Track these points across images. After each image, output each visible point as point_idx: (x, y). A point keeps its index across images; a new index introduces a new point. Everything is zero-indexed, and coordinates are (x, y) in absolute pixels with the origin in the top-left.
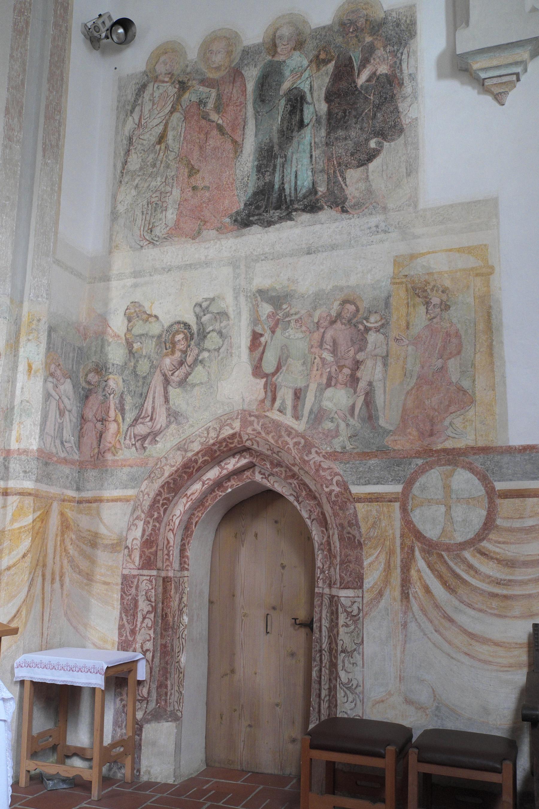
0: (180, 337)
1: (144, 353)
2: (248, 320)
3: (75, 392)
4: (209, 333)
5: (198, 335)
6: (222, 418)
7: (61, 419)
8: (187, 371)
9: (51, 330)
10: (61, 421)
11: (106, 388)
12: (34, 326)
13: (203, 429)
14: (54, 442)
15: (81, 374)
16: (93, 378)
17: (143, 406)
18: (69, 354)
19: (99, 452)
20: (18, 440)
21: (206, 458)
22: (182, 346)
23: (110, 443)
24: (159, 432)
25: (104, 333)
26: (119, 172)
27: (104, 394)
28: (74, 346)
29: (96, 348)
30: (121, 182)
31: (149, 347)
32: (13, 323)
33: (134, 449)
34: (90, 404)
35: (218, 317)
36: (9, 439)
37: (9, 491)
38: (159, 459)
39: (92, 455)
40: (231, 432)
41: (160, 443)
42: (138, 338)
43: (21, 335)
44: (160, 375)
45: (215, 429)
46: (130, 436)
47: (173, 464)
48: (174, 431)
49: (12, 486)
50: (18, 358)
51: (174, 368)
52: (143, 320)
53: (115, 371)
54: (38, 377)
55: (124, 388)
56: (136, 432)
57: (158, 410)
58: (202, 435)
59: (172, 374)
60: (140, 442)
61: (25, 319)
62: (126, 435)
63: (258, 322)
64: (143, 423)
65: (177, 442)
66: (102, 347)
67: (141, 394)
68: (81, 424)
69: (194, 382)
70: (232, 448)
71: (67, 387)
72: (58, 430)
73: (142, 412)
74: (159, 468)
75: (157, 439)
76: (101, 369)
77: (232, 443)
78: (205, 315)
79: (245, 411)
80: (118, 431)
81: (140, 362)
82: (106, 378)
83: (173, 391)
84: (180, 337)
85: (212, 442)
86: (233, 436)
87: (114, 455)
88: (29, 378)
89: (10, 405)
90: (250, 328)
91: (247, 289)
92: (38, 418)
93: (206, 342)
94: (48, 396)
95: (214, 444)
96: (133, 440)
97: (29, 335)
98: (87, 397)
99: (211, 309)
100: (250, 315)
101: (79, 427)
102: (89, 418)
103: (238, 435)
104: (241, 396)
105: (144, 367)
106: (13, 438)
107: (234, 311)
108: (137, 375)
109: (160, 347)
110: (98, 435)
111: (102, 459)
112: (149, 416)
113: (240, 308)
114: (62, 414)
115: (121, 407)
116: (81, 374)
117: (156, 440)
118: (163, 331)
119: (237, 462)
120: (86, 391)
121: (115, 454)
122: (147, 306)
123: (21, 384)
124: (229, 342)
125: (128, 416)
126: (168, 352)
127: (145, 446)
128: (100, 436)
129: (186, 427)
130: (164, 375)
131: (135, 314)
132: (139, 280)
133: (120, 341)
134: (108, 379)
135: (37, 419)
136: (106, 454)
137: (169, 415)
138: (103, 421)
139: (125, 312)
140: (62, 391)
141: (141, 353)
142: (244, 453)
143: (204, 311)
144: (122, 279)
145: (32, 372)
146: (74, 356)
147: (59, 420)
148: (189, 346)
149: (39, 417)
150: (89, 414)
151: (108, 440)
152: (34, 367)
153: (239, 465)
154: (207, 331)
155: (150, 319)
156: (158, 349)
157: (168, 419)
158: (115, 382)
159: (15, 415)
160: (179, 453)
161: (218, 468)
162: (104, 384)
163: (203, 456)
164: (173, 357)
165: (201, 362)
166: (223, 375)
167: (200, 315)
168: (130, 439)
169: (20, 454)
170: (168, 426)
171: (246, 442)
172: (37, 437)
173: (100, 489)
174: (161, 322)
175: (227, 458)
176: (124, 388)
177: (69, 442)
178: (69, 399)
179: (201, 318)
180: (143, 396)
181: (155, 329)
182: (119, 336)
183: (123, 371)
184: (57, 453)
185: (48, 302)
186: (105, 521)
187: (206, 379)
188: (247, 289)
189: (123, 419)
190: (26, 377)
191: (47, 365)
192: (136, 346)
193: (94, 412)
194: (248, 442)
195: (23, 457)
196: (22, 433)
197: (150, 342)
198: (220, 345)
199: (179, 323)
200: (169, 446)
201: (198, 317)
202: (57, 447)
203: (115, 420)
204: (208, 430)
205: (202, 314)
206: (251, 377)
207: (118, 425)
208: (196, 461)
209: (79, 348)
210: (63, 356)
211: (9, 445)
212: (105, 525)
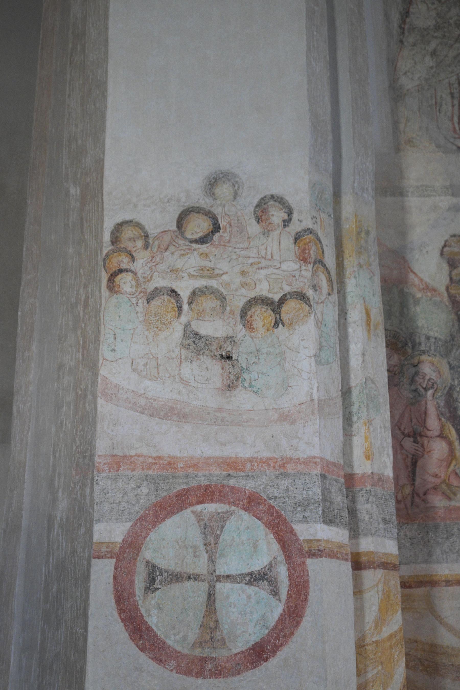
11: (417, 379)
19: (414, 493)
23: (436, 476)
26: (396, 25)
27: (413, 387)
30: (401, 41)
37: (364, 559)
39: (400, 498)
49: (371, 548)
53: (433, 348)
55: (453, 379)
82: (415, 361)
87: (450, 499)
115: (450, 412)
121: (452, 496)
134: (419, 363)
144: (429, 196)
162: (413, 370)
173: (426, 562)
182: (434, 290)
186: (451, 621)
203: (442, 436)
212: (450, 629)
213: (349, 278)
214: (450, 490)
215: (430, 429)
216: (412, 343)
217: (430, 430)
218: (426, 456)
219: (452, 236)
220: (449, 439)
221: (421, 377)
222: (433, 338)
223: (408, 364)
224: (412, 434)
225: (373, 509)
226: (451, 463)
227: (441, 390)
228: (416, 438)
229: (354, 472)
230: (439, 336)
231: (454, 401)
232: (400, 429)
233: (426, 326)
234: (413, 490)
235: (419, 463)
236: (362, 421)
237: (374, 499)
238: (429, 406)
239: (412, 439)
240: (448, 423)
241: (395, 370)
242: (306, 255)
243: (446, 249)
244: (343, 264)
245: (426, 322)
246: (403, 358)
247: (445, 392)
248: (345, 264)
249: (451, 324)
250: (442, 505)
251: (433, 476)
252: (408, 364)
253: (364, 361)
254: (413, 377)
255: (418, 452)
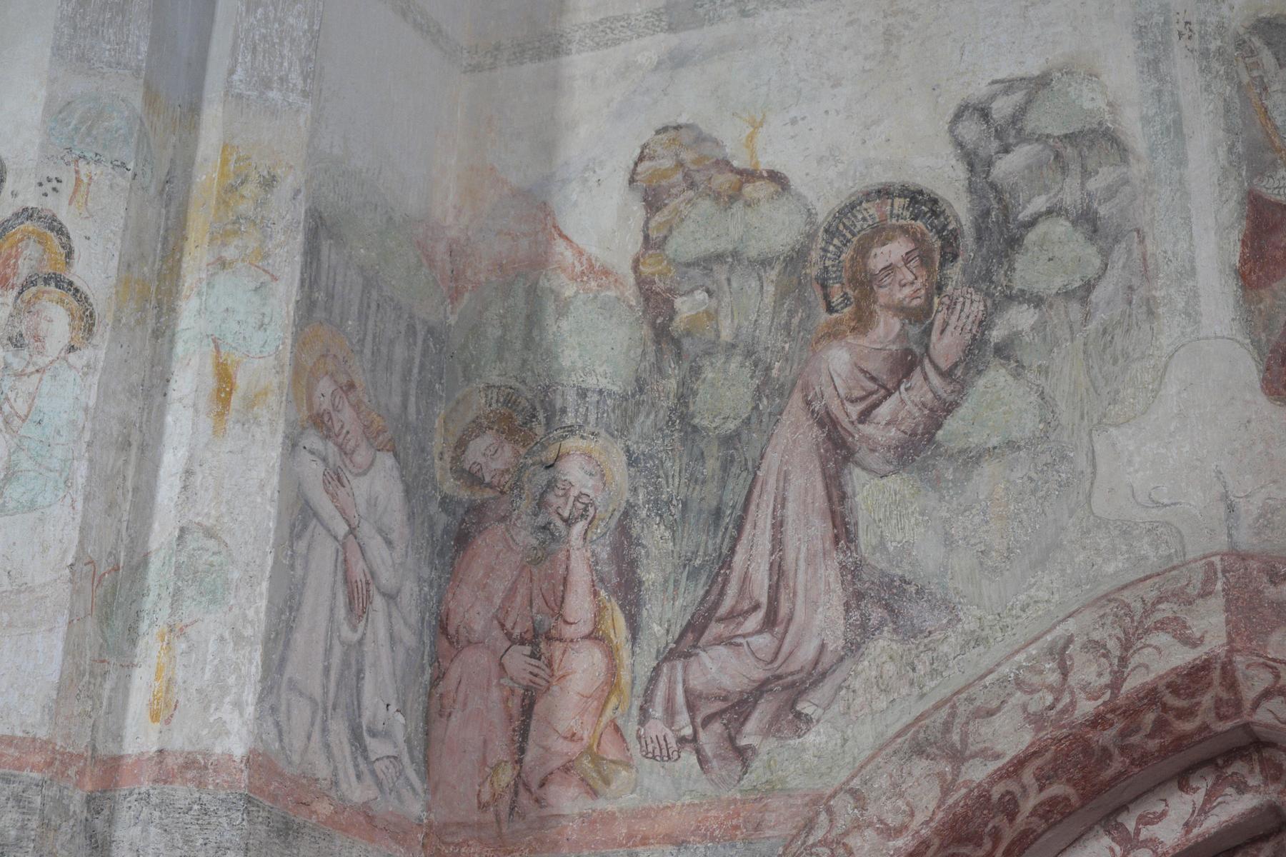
0: (894, 251)
1: (726, 335)
2: (1222, 152)
3: (411, 516)
4: (1032, 223)
5: (979, 239)
6: (1127, 596)
7: (354, 629)
8: (936, 396)
9: (320, 230)
10: (356, 637)
11: (551, 498)
12: (245, 207)
13: (1033, 650)
14: (325, 730)
15: (437, 443)
16: (491, 455)
17: (725, 562)
18: (392, 342)
19: (520, 783)
20: (163, 711)
21: (1057, 789)
22: (907, 291)
23: (572, 737)
24: (816, 675)
25: (539, 262)
27: (541, 520)
28: (411, 317)
29: (505, 327)
31: (749, 307)
32: (152, 191)
33: (689, 758)
34: (477, 571)
35: (1069, 152)
36: (118, 708)
38: (820, 803)
39: (486, 797)
40: (1182, 657)
41: (821, 727)
42: (695, 272)
43: (190, 246)
44: (806, 422)
45: (1096, 647)
46: (670, 700)
47: (892, 820)
48: (890, 668)
50: (172, 342)
51: (871, 386)
52: (717, 197)
53: (592, 418)
54: (259, 424)
55: (635, 490)
56: (697, 683)
57: (800, 578)
58: (1036, 680)
59: (865, 416)
60: (717, 727)
61: (207, 175)
62: (648, 696)
63: (1269, 156)
64: (729, 642)
65: (907, 719)
66: (533, 320)
67: (718, 514)
68: (435, 659)
69: (974, 440)
70: (1184, 736)
71: (379, 485)
72: (342, 675)
73: (722, 593)
74: (824, 842)
75: (805, 707)
76: (527, 417)
77: (1183, 714)
78: (1006, 150)
79: (1243, 557)
80: (612, 682)
81: (709, 374)
82: (550, 455)
83: (869, 492)
84: (894, 251)
85: (1087, 707)
86: (1196, 675)
87: (594, 793)
88: (219, 430)
89: (131, 551)
90: (1232, 184)
91: (1203, 23)
92: (256, 608)
93: (1020, 262)
94: (299, 517)
95: (1097, 721)
96: (683, 718)
97: (224, 244)
98: (463, 539)
99: (1033, 122)
100: (1228, 130)
101: (428, 671)
102: (470, 630)
103: (1216, 675)
104: (1218, 488)
105: (725, 394)
106: (138, 703)
107: (1146, 120)
108: (695, 429)
109: (802, 301)
110: (515, 704)
111: (533, 815)
112: (756, 607)
113: (1176, 106)
114: (357, 604)
115: (620, 574)
116: (437, 443)
117: (798, 715)
118: (811, 236)
119: (1204, 811)
120: (461, 511)
121: (599, 785)
122: (732, 140)
123: (183, 452)
124: (1136, 254)
125: (657, 610)
126: (838, 322)
127: (742, 742)
128: (527, 708)
129: (945, 648)
130: (827, 422)
131: (679, 176)
132: (691, 38)
133: (612, 293)
134: (558, 458)
135: (251, 614)
136: (552, 789)
137: (860, 596)
138: (539, 639)
139: (634, 172)
140: (361, 501)
141: (712, 336)
142: (1238, 767)
143: (999, 134)
144: (616, 42)
145: (235, 401)
146: (410, 360)
147: (346, 631)
148: (940, 288)
149: (263, 604)
150: (474, 614)
151: (562, 727)
152: (241, 382)
153: (1212, 823)
154: (1024, 216)
155: (748, 189)
156: (791, 314)
157: (855, 615)
158: (591, 469)
159: (152, 597)
160: (920, 766)
161: (1106, 841)
162: (543, 477)
163: (1043, 780)
164: (864, 341)
165: (1003, 351)
166: (1115, 401)
167: (982, 152)
168: (670, 713)
169: (165, 778)
170: (853, 648)
171: (1256, 705)
172: (250, 697)
174: (800, 197)
175: (1150, 791)
176: (635, 490)
177: (387, 735)
178: (389, 543)
179: (990, 163)
180: (729, 523)
181: (775, 228)
182: (606, 273)
183: (628, 419)
184: (335, 783)
185: (309, 106)
187: (1031, 424)
188: (1203, 23)
189: (634, 628)
190: (206, 423)
191: (301, 378)
192: (685, 307)
193: (497, 601)
194: (1266, 705)
195: (181, 793)
196: (180, 675)
197: (754, 284)
198: (1091, 273)
199: (884, 193)
200: (865, 737)
201: (974, 162)
202: (335, 750)
203: (595, 636)
204: (1060, 654)
205: (995, 145)
206: (1262, 399)
207: (611, 653)
208: (1009, 807)
209: (431, 331)
210: (367, 352)
211: (118, 737)
213: (188, 297)
214: (599, 773)
215: (571, 620)
216: (546, 410)
217: (566, 622)
218: (555, 688)
219: (658, 132)
220: (611, 641)
221: (561, 493)
222: (594, 391)
223: (533, 464)
224: (528, 636)
225: (145, 838)
226: (606, 703)
227: (603, 520)
228: (538, 645)
229: (125, 752)
230: (610, 387)
231: (631, 544)
232: (502, 626)
233: (579, 365)
234: (519, 775)
235: (538, 708)
236: (156, 630)
237: (157, 814)
238: (573, 564)
239: (527, 649)
240: (613, 600)
241: (503, 482)
242: (8, 271)
243: (646, 165)
244: (180, 267)
245: (580, 356)
246: (522, 451)
247: (613, 523)
248: (184, 265)
249: (639, 351)
250: (576, 811)
251: (565, 738)
252: (533, 464)
253: (185, 488)
254: (542, 495)
255: (537, 680)
